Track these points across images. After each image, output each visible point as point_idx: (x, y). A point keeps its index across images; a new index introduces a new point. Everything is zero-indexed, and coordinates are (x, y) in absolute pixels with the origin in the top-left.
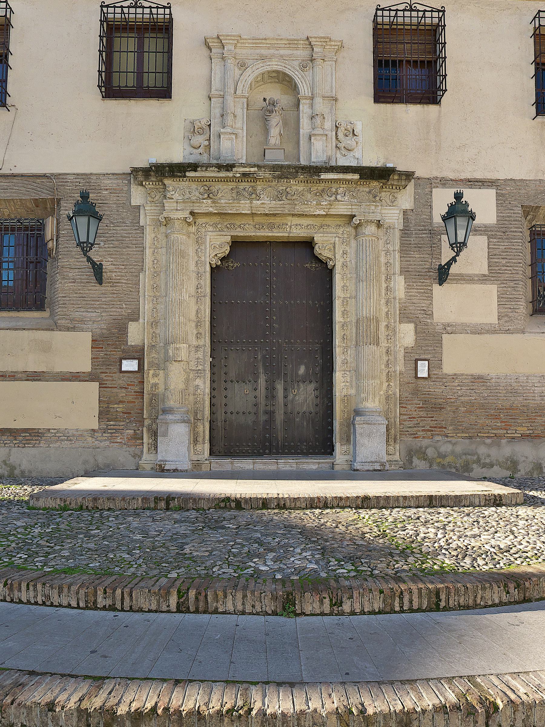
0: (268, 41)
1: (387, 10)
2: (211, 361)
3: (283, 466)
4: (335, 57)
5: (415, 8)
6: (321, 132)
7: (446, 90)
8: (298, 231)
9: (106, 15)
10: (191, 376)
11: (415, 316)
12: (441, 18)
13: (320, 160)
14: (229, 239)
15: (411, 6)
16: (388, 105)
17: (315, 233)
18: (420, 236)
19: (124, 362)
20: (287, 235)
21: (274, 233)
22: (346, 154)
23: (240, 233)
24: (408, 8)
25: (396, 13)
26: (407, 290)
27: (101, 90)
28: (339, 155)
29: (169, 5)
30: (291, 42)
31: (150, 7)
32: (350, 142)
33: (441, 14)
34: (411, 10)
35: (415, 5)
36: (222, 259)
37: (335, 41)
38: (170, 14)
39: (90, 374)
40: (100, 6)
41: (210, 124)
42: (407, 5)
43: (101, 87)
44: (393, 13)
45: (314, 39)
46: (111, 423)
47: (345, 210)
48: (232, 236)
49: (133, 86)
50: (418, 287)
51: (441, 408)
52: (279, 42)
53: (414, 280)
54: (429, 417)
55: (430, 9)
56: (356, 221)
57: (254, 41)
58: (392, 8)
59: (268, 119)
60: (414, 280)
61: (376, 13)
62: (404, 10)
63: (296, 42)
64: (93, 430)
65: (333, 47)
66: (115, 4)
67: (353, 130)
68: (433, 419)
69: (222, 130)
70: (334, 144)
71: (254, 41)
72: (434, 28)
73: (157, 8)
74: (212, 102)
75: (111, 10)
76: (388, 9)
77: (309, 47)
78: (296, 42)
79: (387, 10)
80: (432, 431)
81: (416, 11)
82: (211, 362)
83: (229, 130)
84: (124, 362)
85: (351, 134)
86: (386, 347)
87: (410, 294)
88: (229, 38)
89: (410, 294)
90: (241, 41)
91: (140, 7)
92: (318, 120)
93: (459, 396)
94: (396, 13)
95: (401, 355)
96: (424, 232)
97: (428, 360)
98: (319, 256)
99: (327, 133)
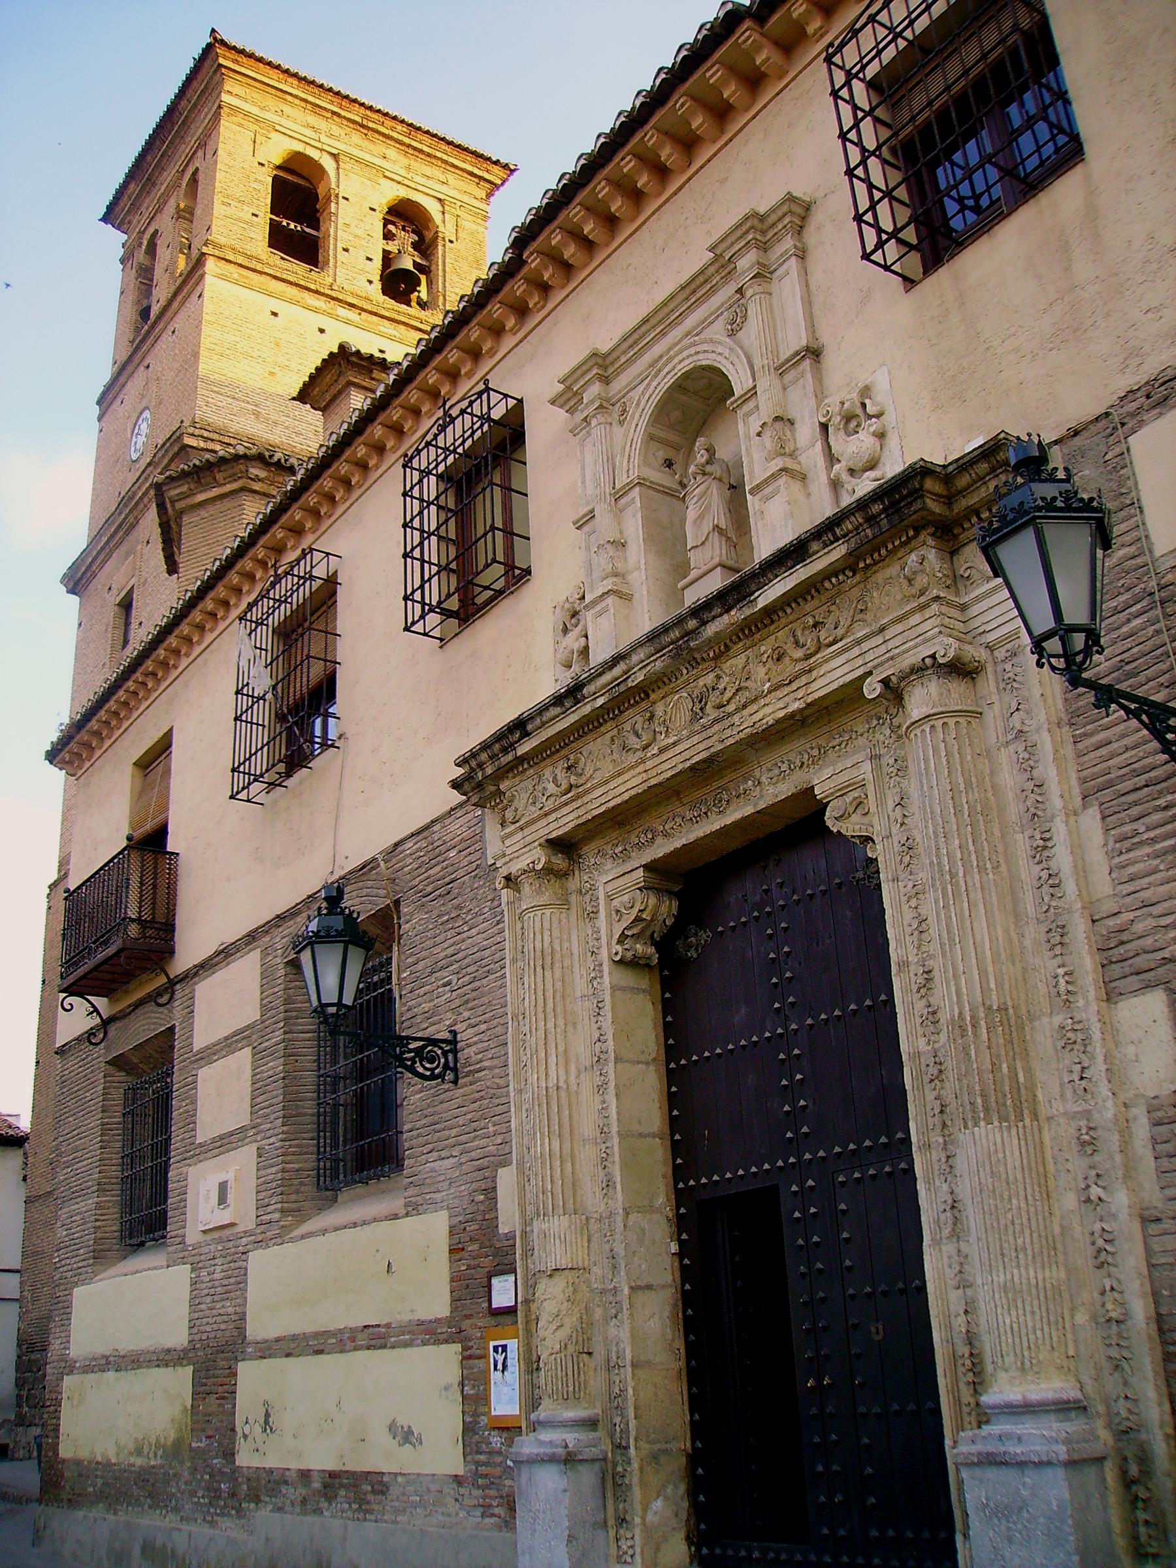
10: (598, 1312)
11: (1159, 955)
18: (1125, 629)
23: (661, 849)
26: (1117, 860)
30: (693, 286)
37: (773, 210)
47: (846, 668)
48: (646, 867)
50: (1152, 834)
53: (1135, 811)
56: (872, 688)
57: (630, 341)
60: (1135, 811)
63: (701, 279)
71: (630, 341)
76: (863, 20)
86: (1073, 1116)
87: (1131, 870)
89: (1131, 870)
90: (608, 362)
96: (1133, 609)
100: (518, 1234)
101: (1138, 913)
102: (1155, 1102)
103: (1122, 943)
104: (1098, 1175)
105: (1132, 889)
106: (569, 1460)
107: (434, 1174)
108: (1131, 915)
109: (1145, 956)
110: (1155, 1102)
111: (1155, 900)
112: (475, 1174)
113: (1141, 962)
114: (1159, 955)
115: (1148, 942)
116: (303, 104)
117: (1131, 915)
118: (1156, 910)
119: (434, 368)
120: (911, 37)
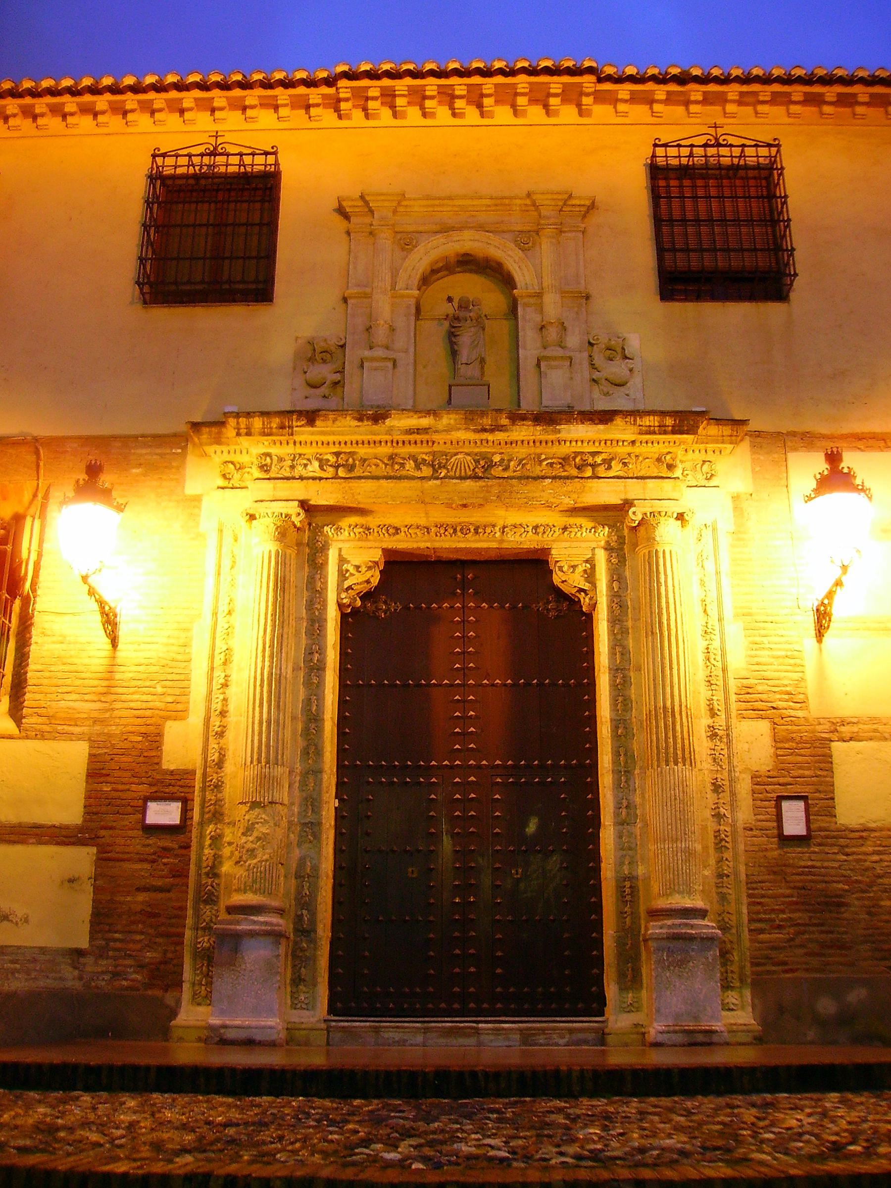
0: (457, 202)
1: (173, 156)
2: (337, 805)
3: (492, 1037)
4: (583, 226)
5: (725, 142)
6: (559, 352)
7: (796, 275)
8: (518, 538)
9: (161, 168)
12: (775, 157)
13: (558, 403)
14: (377, 555)
15: (717, 139)
16: (677, 304)
17: (553, 541)
19: (152, 806)
20: (494, 545)
21: (470, 541)
22: (611, 392)
23: (401, 543)
24: (712, 143)
25: (743, 151)
27: (141, 290)
28: (596, 394)
29: (275, 149)
31: (241, 155)
32: (617, 369)
33: (774, 150)
34: (719, 145)
35: (724, 137)
36: (366, 596)
37: (580, 198)
38: (277, 164)
39: (81, 829)
40: (152, 155)
41: (345, 344)
42: (711, 138)
43: (144, 284)
44: (685, 151)
45: (539, 196)
46: (117, 935)
49: (202, 282)
51: (840, 905)
52: (475, 202)
54: (815, 925)
55: (753, 143)
58: (682, 143)
59: (458, 333)
61: (654, 152)
62: (706, 146)
64: (79, 953)
65: (578, 209)
66: (178, 152)
67: (623, 349)
68: (823, 928)
69: (367, 353)
70: (587, 375)
72: (764, 173)
73: (253, 154)
74: (350, 306)
75: (170, 161)
76: (675, 144)
77: (533, 208)
78: (507, 201)
79: (173, 156)
80: (824, 955)
81: (728, 146)
82: (336, 808)
83: (379, 353)
84: (152, 806)
85: (619, 356)
88: (382, 198)
91: (221, 154)
92: (552, 334)
93: (880, 877)
94: (743, 151)
95: (744, 787)
97: (804, 798)
98: (562, 587)
99: (572, 354)
100: (199, 775)
101: (760, 681)
102: (757, 773)
103: (748, 693)
104: (305, 373)
105: (758, 669)
106: (276, 936)
107: (74, 711)
108: (756, 682)
109: (760, 703)
110: (757, 773)
111: (770, 678)
112: (132, 720)
113: (759, 705)
114: (770, 704)
115: (764, 697)
116: (418, 336)
117: (756, 682)
118: (770, 682)
119: (227, 97)
120: (695, 162)
